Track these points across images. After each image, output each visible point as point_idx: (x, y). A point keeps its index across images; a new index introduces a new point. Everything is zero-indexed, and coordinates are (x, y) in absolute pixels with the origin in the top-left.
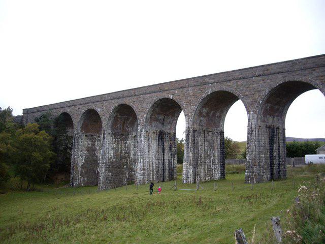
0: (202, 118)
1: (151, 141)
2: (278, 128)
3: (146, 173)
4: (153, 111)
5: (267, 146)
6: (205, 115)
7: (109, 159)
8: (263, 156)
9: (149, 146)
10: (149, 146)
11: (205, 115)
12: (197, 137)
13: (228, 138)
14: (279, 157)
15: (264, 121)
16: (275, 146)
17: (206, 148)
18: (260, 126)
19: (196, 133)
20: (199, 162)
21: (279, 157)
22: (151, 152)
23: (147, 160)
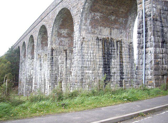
0: (62, 39)
1: (44, 62)
2: (121, 42)
3: (38, 87)
4: (42, 38)
5: (100, 61)
6: (66, 35)
7: (29, 76)
8: (91, 72)
9: (41, 65)
10: (41, 65)
11: (66, 35)
12: (57, 55)
13: (10, 48)
14: (122, 73)
15: (93, 33)
16: (115, 62)
17: (68, 65)
18: (84, 38)
19: (54, 53)
20: (59, 78)
21: (122, 73)
22: (42, 70)
23: (39, 77)
